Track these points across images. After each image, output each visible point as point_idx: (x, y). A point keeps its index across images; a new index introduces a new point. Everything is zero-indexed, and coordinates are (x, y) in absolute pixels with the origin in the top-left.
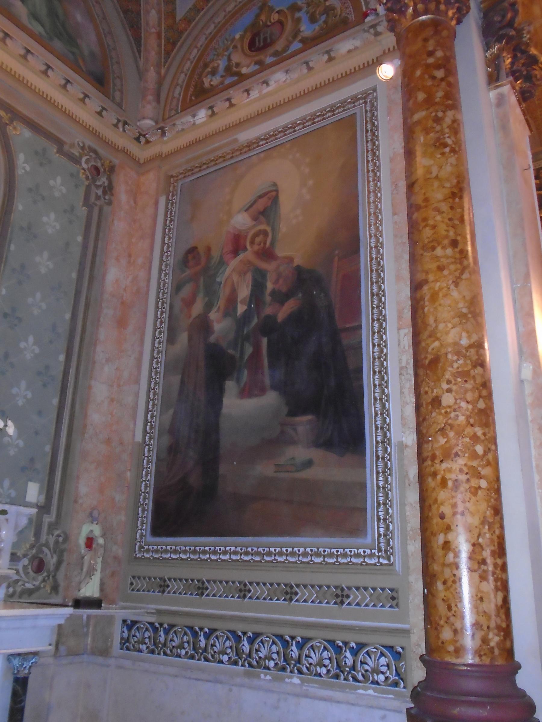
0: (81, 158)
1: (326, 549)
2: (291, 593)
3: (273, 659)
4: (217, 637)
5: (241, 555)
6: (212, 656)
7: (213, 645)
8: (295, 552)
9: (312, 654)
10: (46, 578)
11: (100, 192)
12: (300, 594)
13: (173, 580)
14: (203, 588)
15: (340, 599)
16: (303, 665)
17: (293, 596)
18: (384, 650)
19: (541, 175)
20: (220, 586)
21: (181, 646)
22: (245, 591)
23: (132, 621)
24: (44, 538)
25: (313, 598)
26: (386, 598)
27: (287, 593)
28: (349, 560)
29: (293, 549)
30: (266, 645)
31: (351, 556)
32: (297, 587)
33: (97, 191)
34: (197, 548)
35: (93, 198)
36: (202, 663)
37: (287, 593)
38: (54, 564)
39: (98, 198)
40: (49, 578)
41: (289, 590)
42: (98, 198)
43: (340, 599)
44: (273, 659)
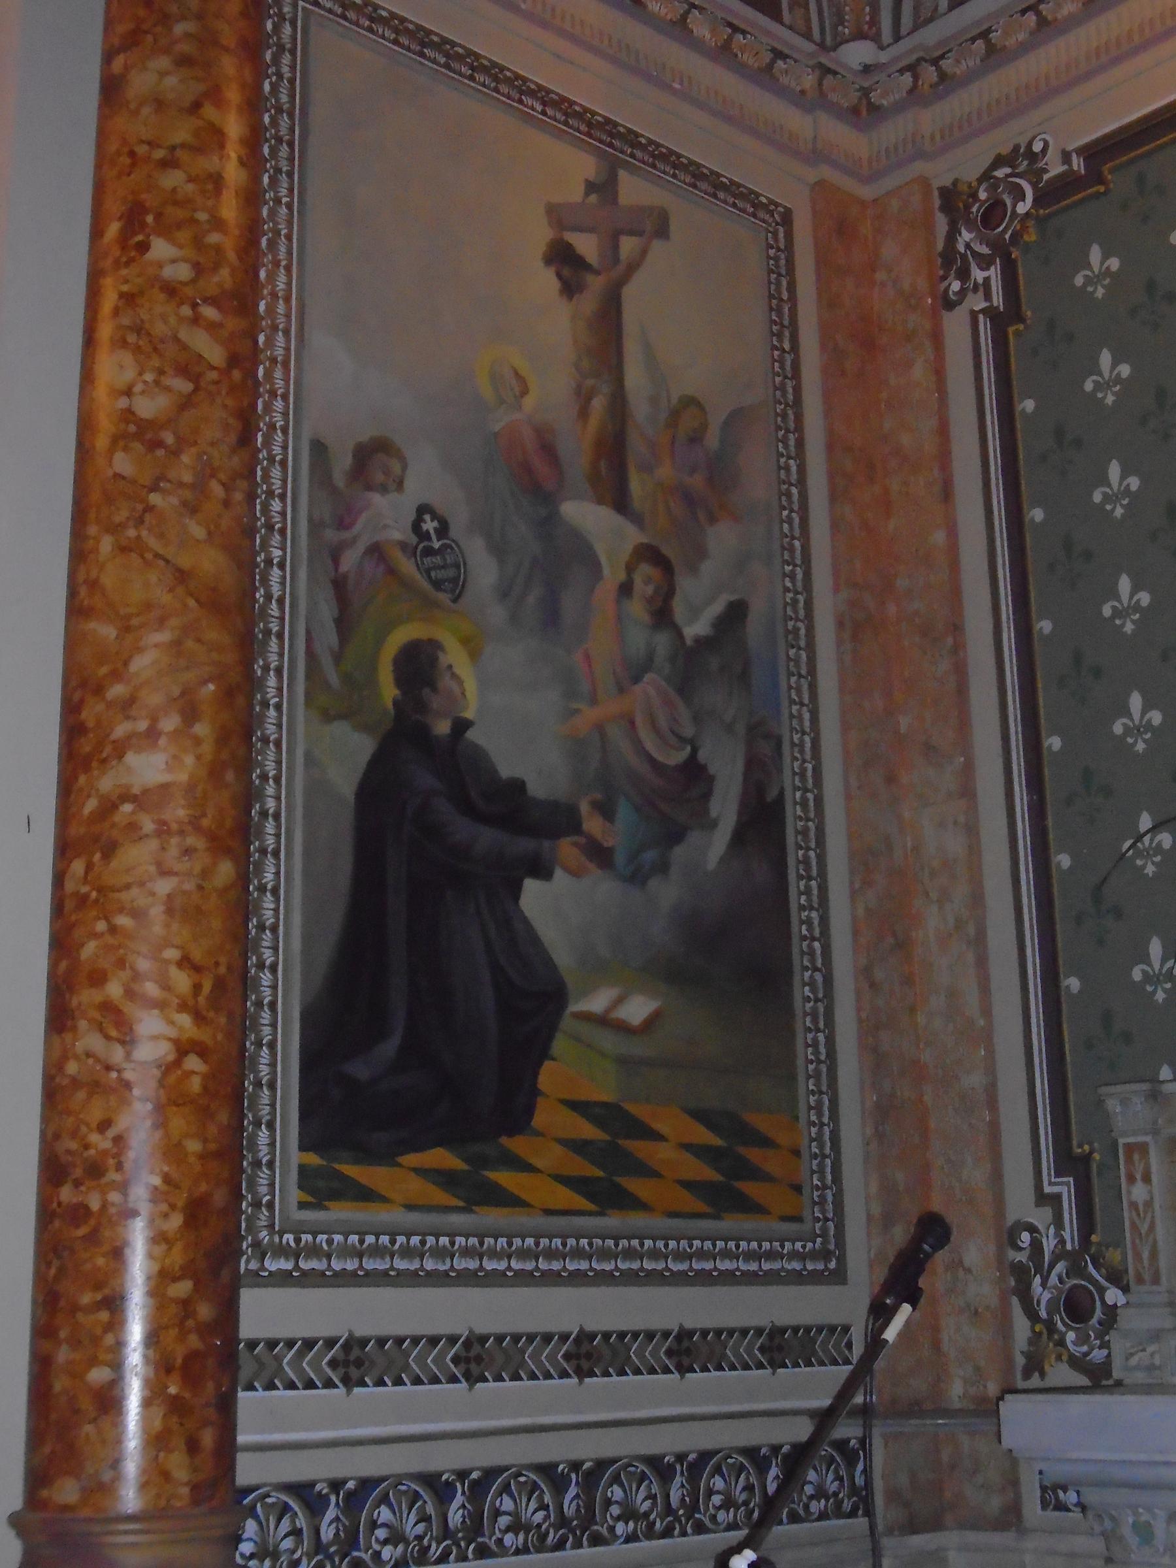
2: (468, 1360)
5: (590, 1258)
14: (578, 1356)
28: (356, 1265)
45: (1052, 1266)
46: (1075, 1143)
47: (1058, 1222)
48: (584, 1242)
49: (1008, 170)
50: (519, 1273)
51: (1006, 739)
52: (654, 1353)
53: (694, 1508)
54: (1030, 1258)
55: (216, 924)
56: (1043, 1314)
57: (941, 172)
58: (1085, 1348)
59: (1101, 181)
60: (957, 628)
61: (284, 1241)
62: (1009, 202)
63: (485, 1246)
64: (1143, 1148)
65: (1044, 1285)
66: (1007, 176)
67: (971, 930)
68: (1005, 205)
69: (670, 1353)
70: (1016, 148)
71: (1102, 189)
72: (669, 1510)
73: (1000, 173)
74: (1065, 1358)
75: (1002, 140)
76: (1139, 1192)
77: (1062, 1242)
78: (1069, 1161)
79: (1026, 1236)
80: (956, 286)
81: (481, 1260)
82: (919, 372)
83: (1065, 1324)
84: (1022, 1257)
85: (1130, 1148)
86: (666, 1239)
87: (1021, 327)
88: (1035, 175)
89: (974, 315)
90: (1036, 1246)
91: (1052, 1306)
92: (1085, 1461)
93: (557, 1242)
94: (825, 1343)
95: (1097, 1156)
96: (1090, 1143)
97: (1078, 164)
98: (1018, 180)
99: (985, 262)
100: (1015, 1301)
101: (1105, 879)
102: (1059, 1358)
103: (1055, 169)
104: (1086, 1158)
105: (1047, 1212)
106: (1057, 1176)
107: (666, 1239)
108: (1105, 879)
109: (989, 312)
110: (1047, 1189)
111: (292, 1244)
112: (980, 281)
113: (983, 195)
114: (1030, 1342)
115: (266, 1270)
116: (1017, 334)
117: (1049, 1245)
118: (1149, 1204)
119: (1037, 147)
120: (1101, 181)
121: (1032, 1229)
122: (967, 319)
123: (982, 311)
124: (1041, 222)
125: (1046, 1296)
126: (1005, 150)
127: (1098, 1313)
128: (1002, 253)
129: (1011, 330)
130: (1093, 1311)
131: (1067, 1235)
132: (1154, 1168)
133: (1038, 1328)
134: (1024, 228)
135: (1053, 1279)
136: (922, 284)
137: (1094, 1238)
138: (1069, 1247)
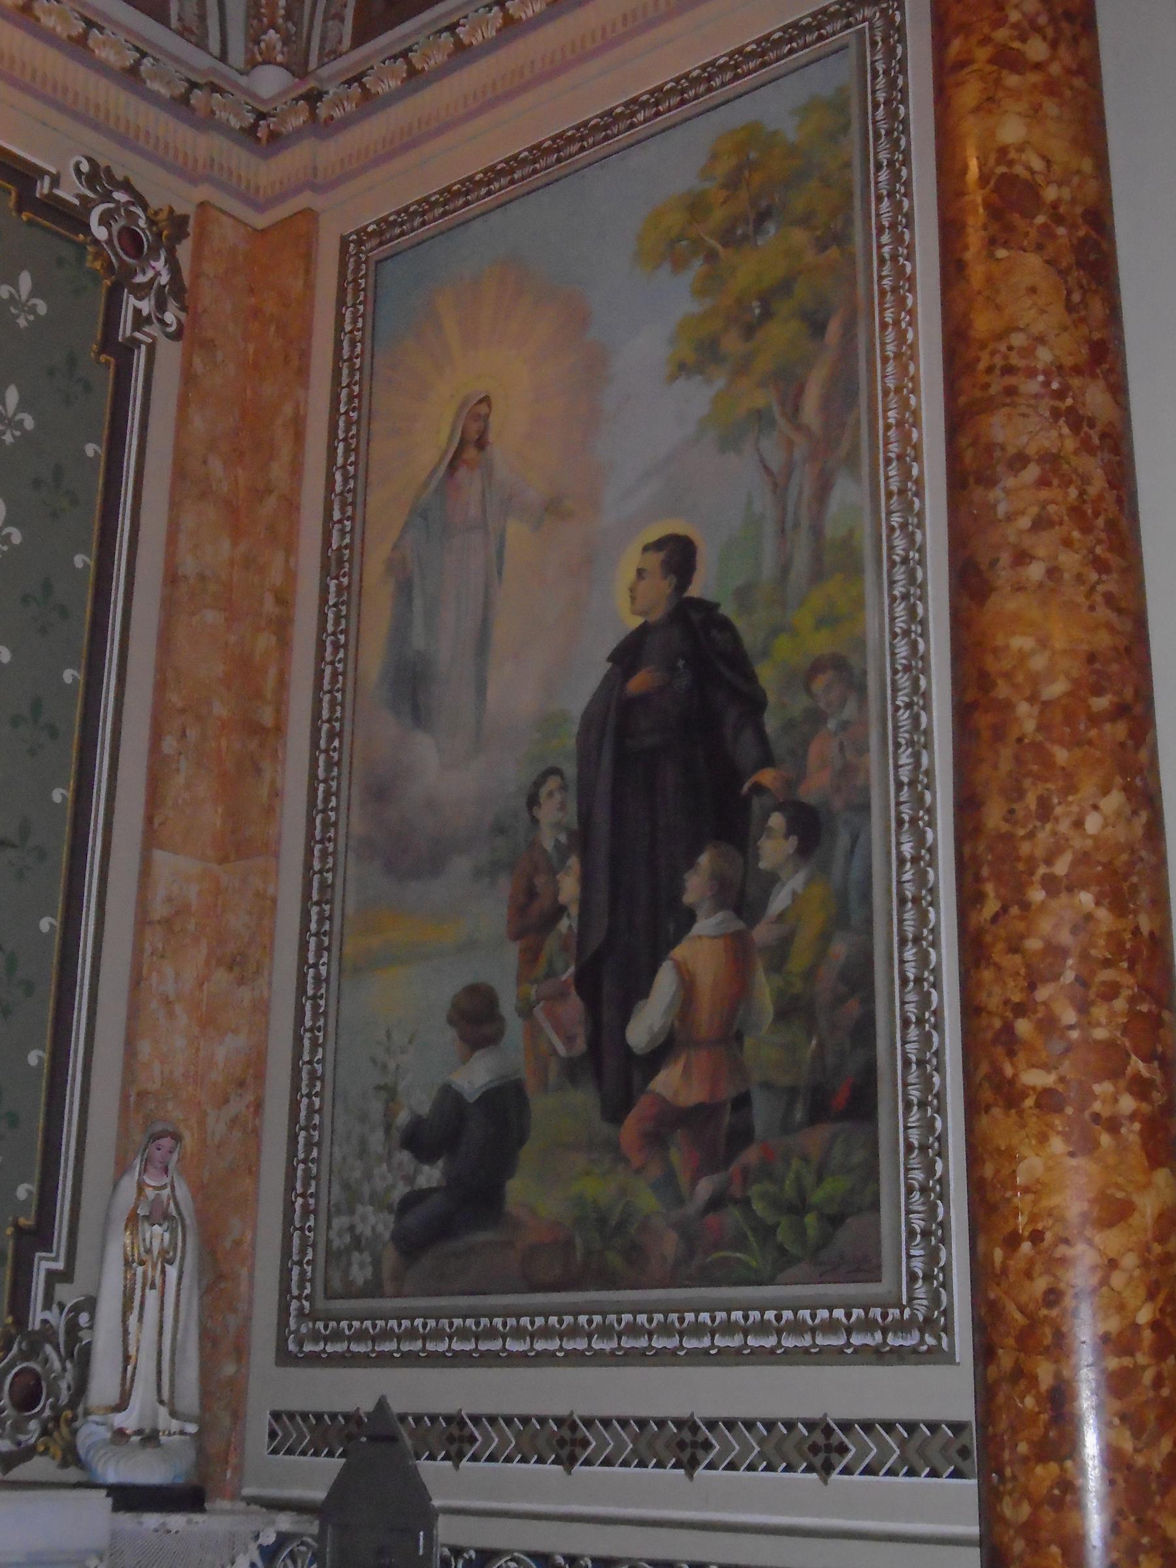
0: (87, 205)
1: (354, 1323)
2: (828, 1448)
5: (590, 1337)
8: (769, 1321)
10: (50, 1425)
11: (146, 306)
12: (594, 1444)
13: (285, 1418)
14: (461, 1439)
15: (822, 1456)
17: (700, 1453)
20: (607, 1435)
22: (694, 1444)
23: (479, 1551)
24: (37, 1316)
25: (751, 1458)
26: (667, 1445)
27: (451, 1439)
28: (345, 1348)
29: (795, 1314)
31: (681, 1334)
32: (623, 1427)
33: (139, 304)
34: (498, 1321)
35: (126, 328)
37: (682, 1445)
38: (69, 1388)
39: (140, 321)
40: (57, 1426)
41: (687, 1436)
42: (140, 321)
43: (822, 1456)
48: (553, 1320)
50: (691, 1352)
51: (144, 426)
52: (488, 1440)
61: (669, 1320)
63: (853, 1319)
69: (585, 1443)
81: (650, 1339)
86: (681, 1311)
93: (839, 1313)
94: (301, 1436)
101: (765, 466)
107: (399, 1319)
108: (765, 466)
111: (396, 1328)
115: (684, 1348)
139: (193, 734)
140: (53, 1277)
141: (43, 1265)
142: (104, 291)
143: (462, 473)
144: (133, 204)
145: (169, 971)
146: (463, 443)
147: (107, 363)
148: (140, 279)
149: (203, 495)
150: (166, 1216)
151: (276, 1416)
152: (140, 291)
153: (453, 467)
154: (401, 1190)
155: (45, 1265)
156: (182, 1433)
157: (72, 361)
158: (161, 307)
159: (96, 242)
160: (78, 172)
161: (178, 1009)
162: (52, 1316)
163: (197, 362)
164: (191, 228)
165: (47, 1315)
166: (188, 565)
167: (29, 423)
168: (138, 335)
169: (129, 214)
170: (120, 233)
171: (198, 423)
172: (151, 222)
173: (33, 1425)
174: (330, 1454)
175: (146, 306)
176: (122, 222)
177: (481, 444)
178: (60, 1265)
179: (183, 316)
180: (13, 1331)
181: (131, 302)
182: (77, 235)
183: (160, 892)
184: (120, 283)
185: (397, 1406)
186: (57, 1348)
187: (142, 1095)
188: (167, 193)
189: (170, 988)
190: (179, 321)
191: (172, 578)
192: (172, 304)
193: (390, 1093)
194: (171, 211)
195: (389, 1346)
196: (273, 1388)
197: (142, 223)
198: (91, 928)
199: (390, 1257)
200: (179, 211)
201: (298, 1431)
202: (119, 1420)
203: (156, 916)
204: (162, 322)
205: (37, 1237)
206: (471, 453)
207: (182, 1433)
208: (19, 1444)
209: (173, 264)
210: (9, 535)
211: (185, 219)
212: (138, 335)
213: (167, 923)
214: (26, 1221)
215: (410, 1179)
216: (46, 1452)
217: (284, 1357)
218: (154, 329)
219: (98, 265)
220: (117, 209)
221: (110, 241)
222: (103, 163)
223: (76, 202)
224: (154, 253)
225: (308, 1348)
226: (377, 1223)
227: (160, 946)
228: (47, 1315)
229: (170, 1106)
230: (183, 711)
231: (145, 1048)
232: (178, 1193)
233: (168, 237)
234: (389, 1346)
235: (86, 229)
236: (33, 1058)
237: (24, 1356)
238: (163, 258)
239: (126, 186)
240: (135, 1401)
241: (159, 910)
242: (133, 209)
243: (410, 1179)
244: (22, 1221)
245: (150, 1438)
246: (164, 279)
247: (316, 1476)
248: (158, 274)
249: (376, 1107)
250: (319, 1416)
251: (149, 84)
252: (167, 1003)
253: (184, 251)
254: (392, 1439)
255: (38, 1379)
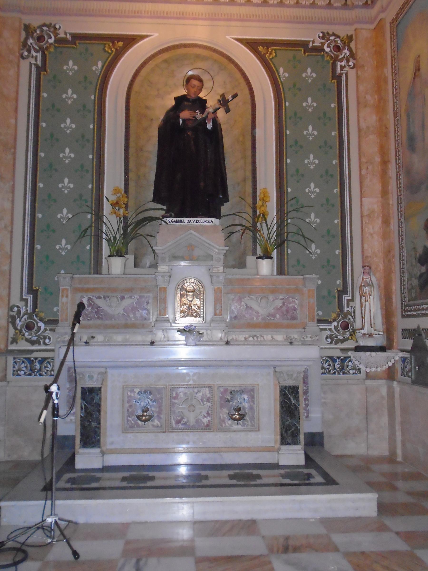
0: (323, 44)
3: (23, 370)
4: (49, 362)
6: (46, 373)
7: (45, 367)
9: (49, 366)
16: (43, 372)
18: (25, 360)
19: (242, 1)
21: (20, 370)
23: (42, 358)
30: (18, 364)
33: (341, 64)
35: (338, 71)
36: (38, 377)
39: (342, 68)
42: (342, 68)
44: (23, 370)
45: (23, 316)
46: (34, 287)
47: (26, 306)
49: (47, 29)
53: (343, 368)
54: (17, 314)
55: (382, 234)
56: (19, 328)
57: (28, 19)
58: (30, 337)
59: (75, 44)
60: (15, 147)
62: (46, 38)
64: (67, 290)
65: (20, 321)
66: (47, 30)
67: (10, 229)
68: (45, 38)
70: (51, 24)
71: (75, 47)
72: (335, 369)
73: (45, 28)
74: (24, 339)
75: (48, 20)
76: (64, 300)
77: (27, 310)
78: (32, 290)
79: (16, 309)
80: (26, 53)
82: (12, 73)
83: (25, 331)
84: (14, 314)
85: (63, 290)
87: (46, 73)
88: (56, 35)
89: (31, 64)
90: (19, 312)
91: (22, 326)
92: (122, 361)
95: (40, 290)
96: (39, 287)
97: (69, 37)
98: (50, 33)
99: (37, 51)
100: (10, 325)
102: (22, 339)
103: (62, 35)
104: (37, 291)
105: (23, 303)
106: (27, 294)
109: (36, 65)
110: (24, 297)
112: (34, 55)
113: (38, 32)
114: (14, 335)
116: (44, 74)
117: (23, 311)
118: (67, 303)
119: (57, 27)
120: (75, 44)
121: (18, 307)
122: (28, 65)
123: (34, 64)
124: (56, 48)
125: (20, 324)
126: (47, 23)
127: (36, 328)
128: (43, 51)
129: (42, 73)
130: (34, 328)
131: (28, 309)
132: (69, 294)
133: (17, 331)
134: (50, 46)
135: (23, 319)
136: (16, 49)
137: (37, 310)
138: (29, 312)
139: (370, 168)
140: (348, 301)
141: (345, 298)
142: (331, 64)
143: (416, 79)
144: (336, 38)
145: (371, 227)
146: (416, 70)
147: (334, 82)
148: (341, 57)
149: (365, 106)
150: (369, 285)
151: (402, 330)
152: (341, 60)
153: (414, 78)
154: (419, 274)
155: (346, 298)
156: (379, 334)
157: (324, 85)
158: (348, 61)
159: (327, 53)
160: (319, 37)
161: (374, 235)
162: (349, 309)
163: (359, 73)
164: (354, 37)
165: (348, 309)
166: (363, 125)
167: (315, 104)
168: (342, 72)
169: (335, 41)
170: (333, 48)
171: (361, 88)
172: (342, 41)
173: (347, 333)
174: (412, 339)
175: (343, 64)
176: (333, 44)
177: (419, 70)
178: (350, 298)
179: (355, 62)
180: (340, 313)
181: (339, 64)
182: (321, 53)
183: (365, 208)
184: (335, 60)
185: (422, 327)
186: (352, 316)
187: (367, 257)
188: (344, 31)
189: (372, 231)
190: (354, 64)
191: (360, 130)
192: (351, 59)
193: (415, 249)
194: (347, 35)
195: (419, 312)
196: (402, 323)
197: (339, 42)
198: (349, 220)
199: (418, 290)
200: (350, 34)
201: (408, 333)
202: (362, 331)
203: (365, 214)
204: (349, 66)
205: (344, 291)
206: (417, 73)
207: (379, 334)
208: (344, 337)
209: (350, 50)
210: (314, 133)
211: (352, 36)
212: (342, 72)
213: (369, 216)
214: (340, 289)
215: (420, 270)
216: (352, 339)
217: (403, 316)
218: (347, 68)
219: (328, 58)
220: (332, 42)
221: (331, 51)
222: (326, 32)
223: (320, 45)
224: (344, 48)
225: (407, 313)
226: (415, 282)
227: (367, 221)
228: (348, 309)
229: (375, 259)
230: (366, 163)
231: (366, 246)
232: (372, 279)
233: (347, 43)
234: (419, 312)
235: (323, 50)
236: (337, 252)
237: (343, 318)
238: (346, 49)
239: (334, 34)
240: (366, 327)
241: (366, 213)
242: (336, 40)
243: (420, 270)
244: (339, 289)
245: (371, 335)
246: (348, 54)
247: (409, 344)
248: (346, 54)
249: (413, 253)
250: (409, 330)
251: (334, 5)
252: (371, 235)
253: (352, 45)
254: (420, 335)
255: (348, 323)
